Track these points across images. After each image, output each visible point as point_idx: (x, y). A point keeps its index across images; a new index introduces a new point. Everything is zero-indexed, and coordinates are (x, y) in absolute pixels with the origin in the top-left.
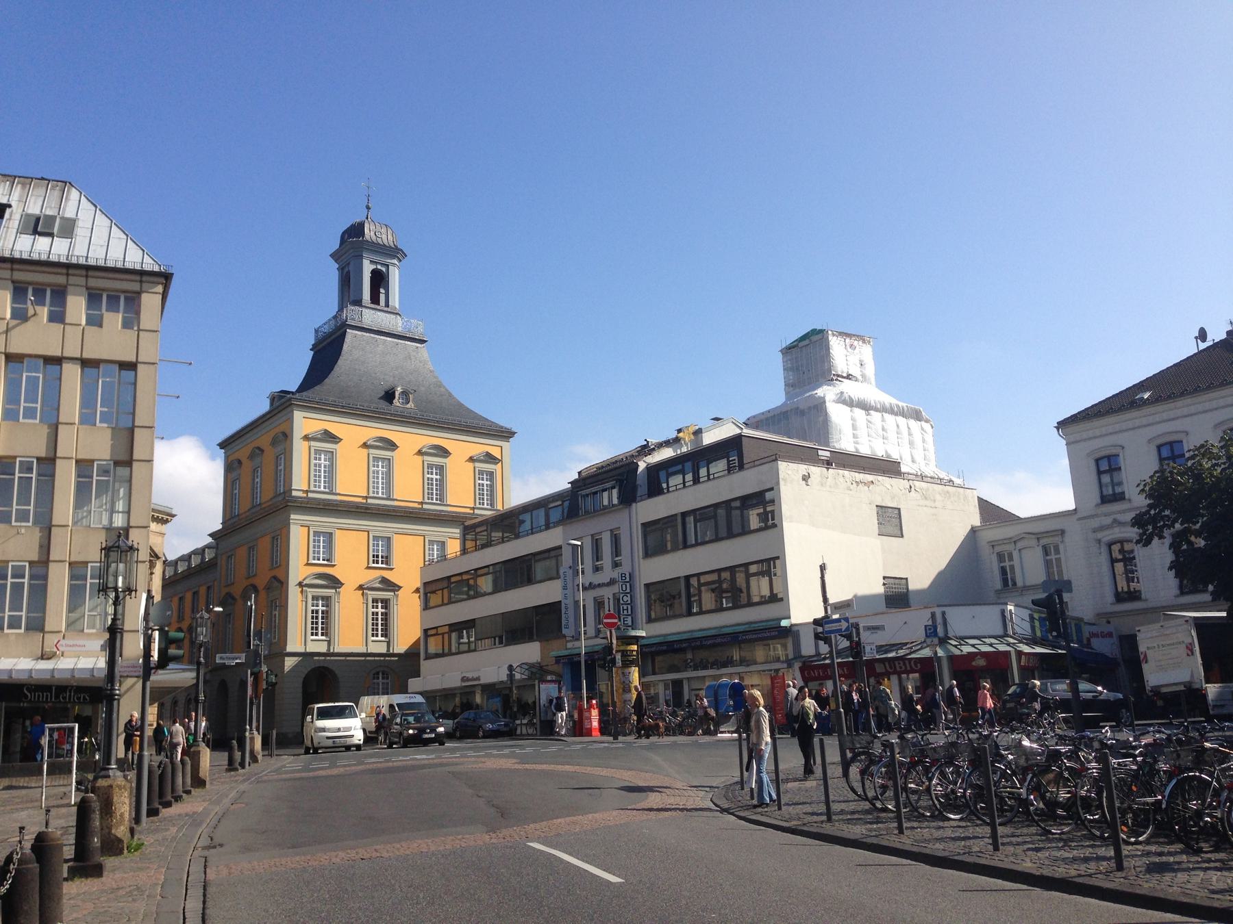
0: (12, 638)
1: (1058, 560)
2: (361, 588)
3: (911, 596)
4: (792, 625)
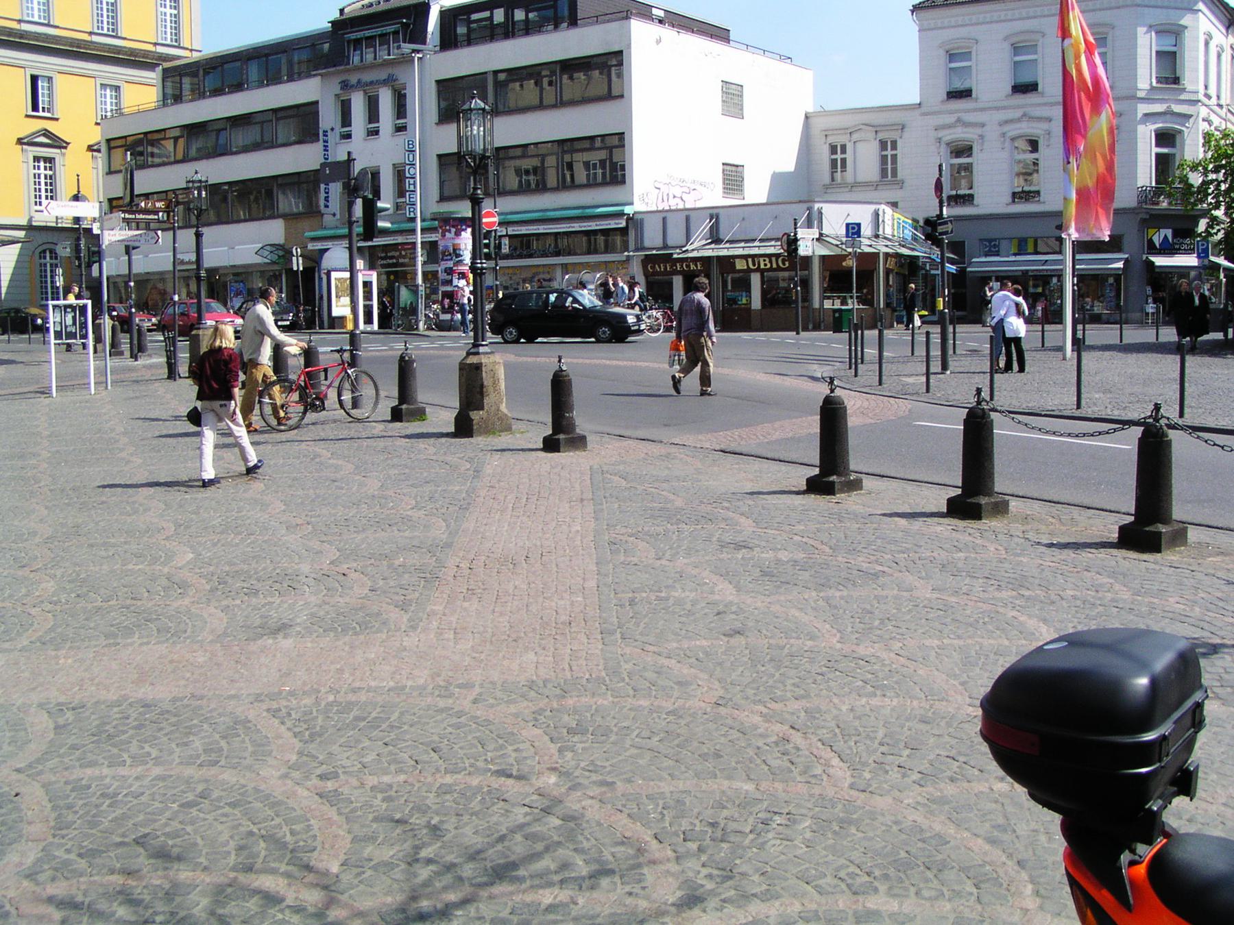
1: (894, 157)
2: (20, 141)
3: (1115, 233)
4: (635, 213)
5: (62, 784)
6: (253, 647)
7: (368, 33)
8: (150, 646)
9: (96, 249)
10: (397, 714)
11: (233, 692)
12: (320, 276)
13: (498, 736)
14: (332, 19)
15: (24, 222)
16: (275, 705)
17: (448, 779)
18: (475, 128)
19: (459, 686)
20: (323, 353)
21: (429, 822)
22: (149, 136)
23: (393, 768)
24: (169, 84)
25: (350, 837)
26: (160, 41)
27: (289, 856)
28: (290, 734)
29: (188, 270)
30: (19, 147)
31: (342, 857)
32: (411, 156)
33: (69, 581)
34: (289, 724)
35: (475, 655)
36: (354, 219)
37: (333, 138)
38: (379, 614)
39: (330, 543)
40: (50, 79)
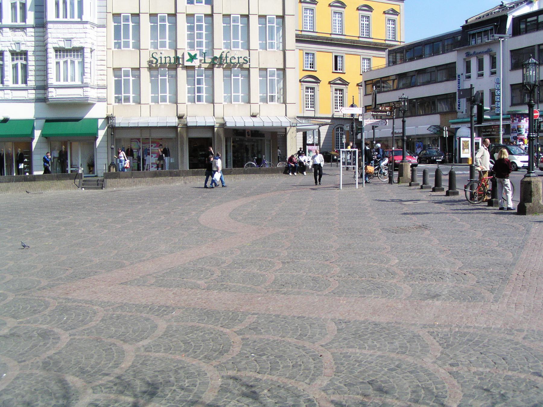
0: (237, 106)
2: (330, 83)
5: (339, 354)
6: (423, 303)
7: (478, 31)
8: (378, 299)
9: (360, 127)
10: (487, 340)
11: (413, 322)
12: (455, 140)
13: (535, 356)
14: (462, 25)
15: (330, 116)
16: (432, 330)
17: (510, 373)
18: (531, 72)
19: (517, 330)
20: (458, 174)
21: (500, 392)
22: (382, 79)
23: (484, 364)
24: (391, 57)
25: (462, 394)
26: (387, 39)
27: (434, 398)
28: (438, 344)
29: (398, 136)
30: (329, 85)
31: (458, 403)
32: (498, 85)
33: (345, 268)
34: (438, 339)
35: (525, 316)
36: (473, 114)
37: (462, 78)
38: (480, 293)
39: (458, 259)
40: (342, 57)
